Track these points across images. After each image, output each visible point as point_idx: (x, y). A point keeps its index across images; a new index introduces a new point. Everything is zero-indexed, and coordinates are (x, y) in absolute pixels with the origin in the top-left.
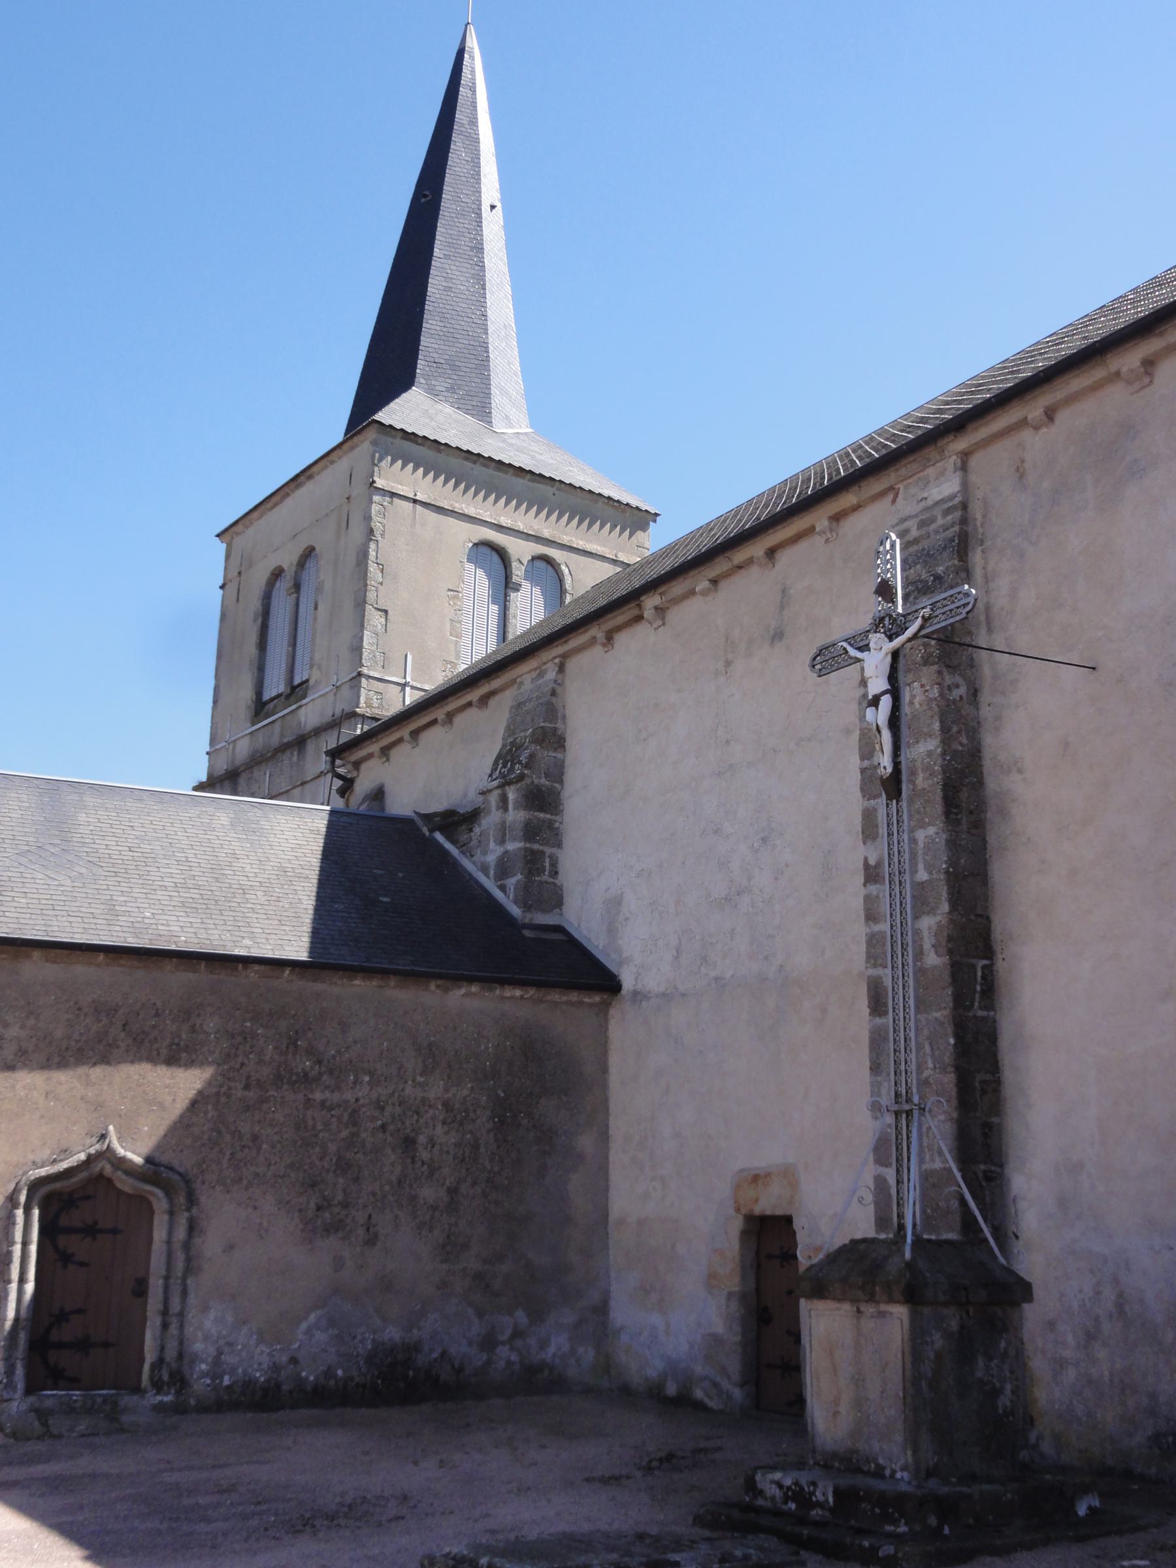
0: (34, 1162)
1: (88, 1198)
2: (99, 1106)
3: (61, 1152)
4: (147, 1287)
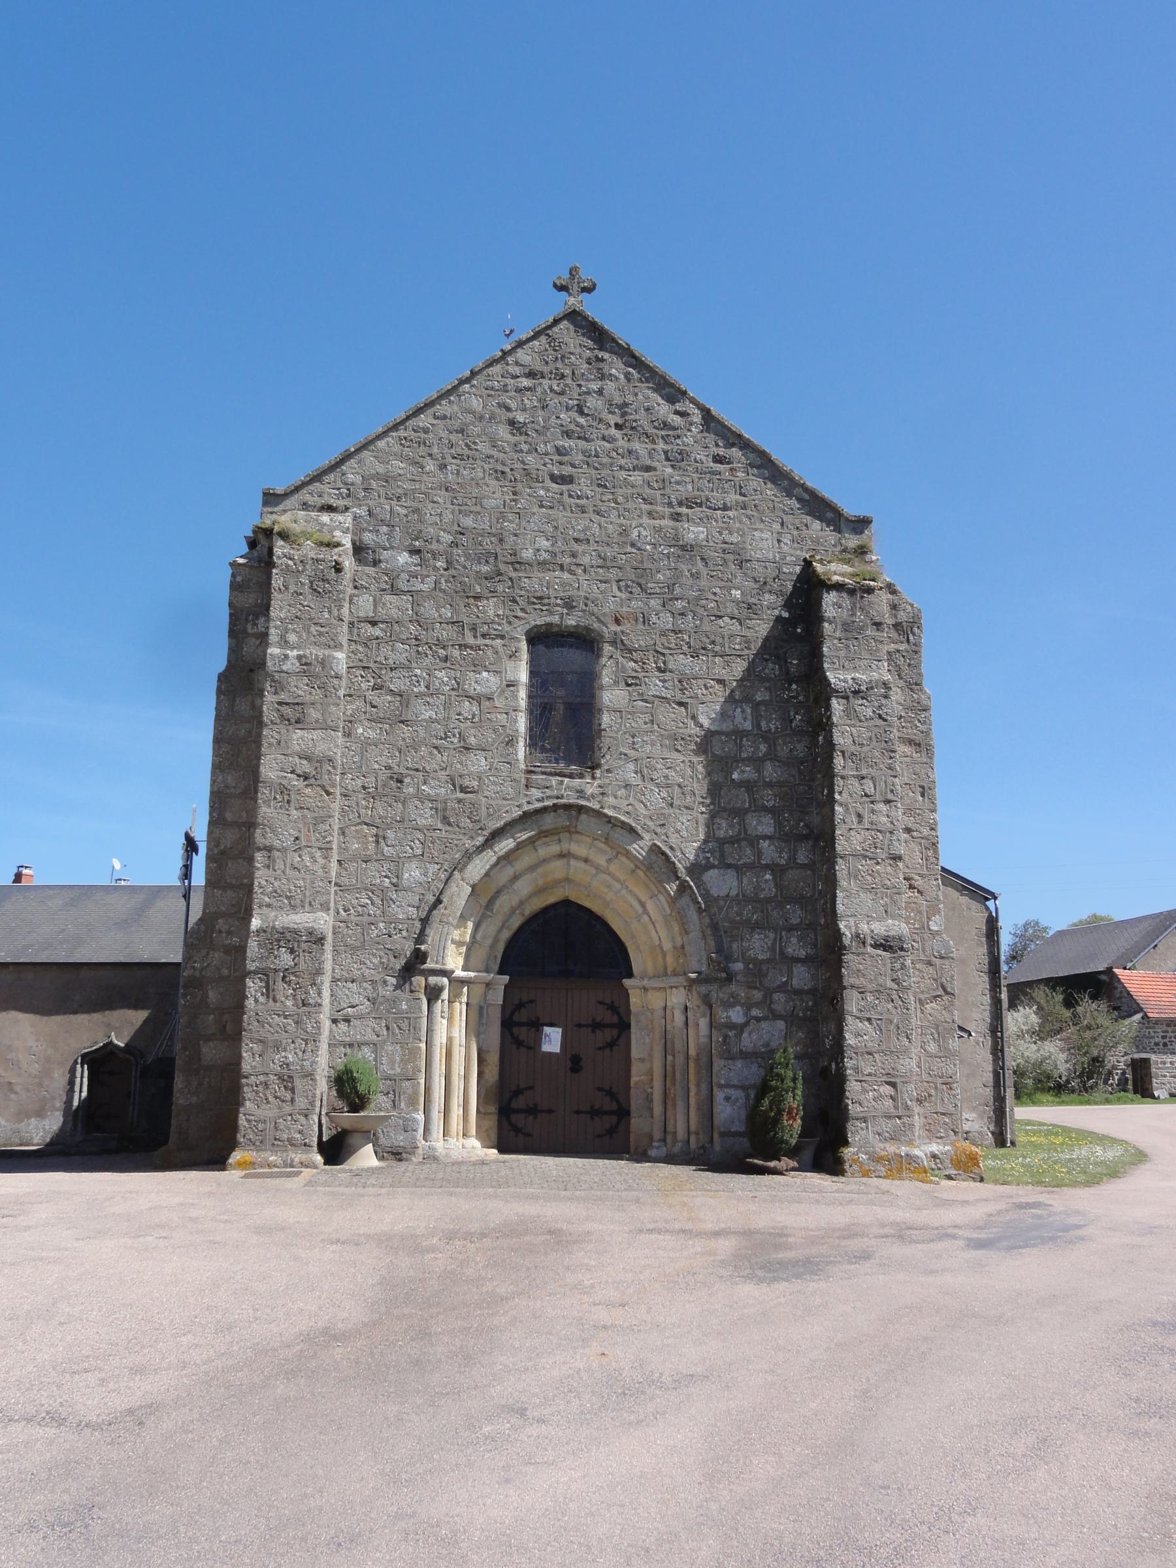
2: (108, 1025)
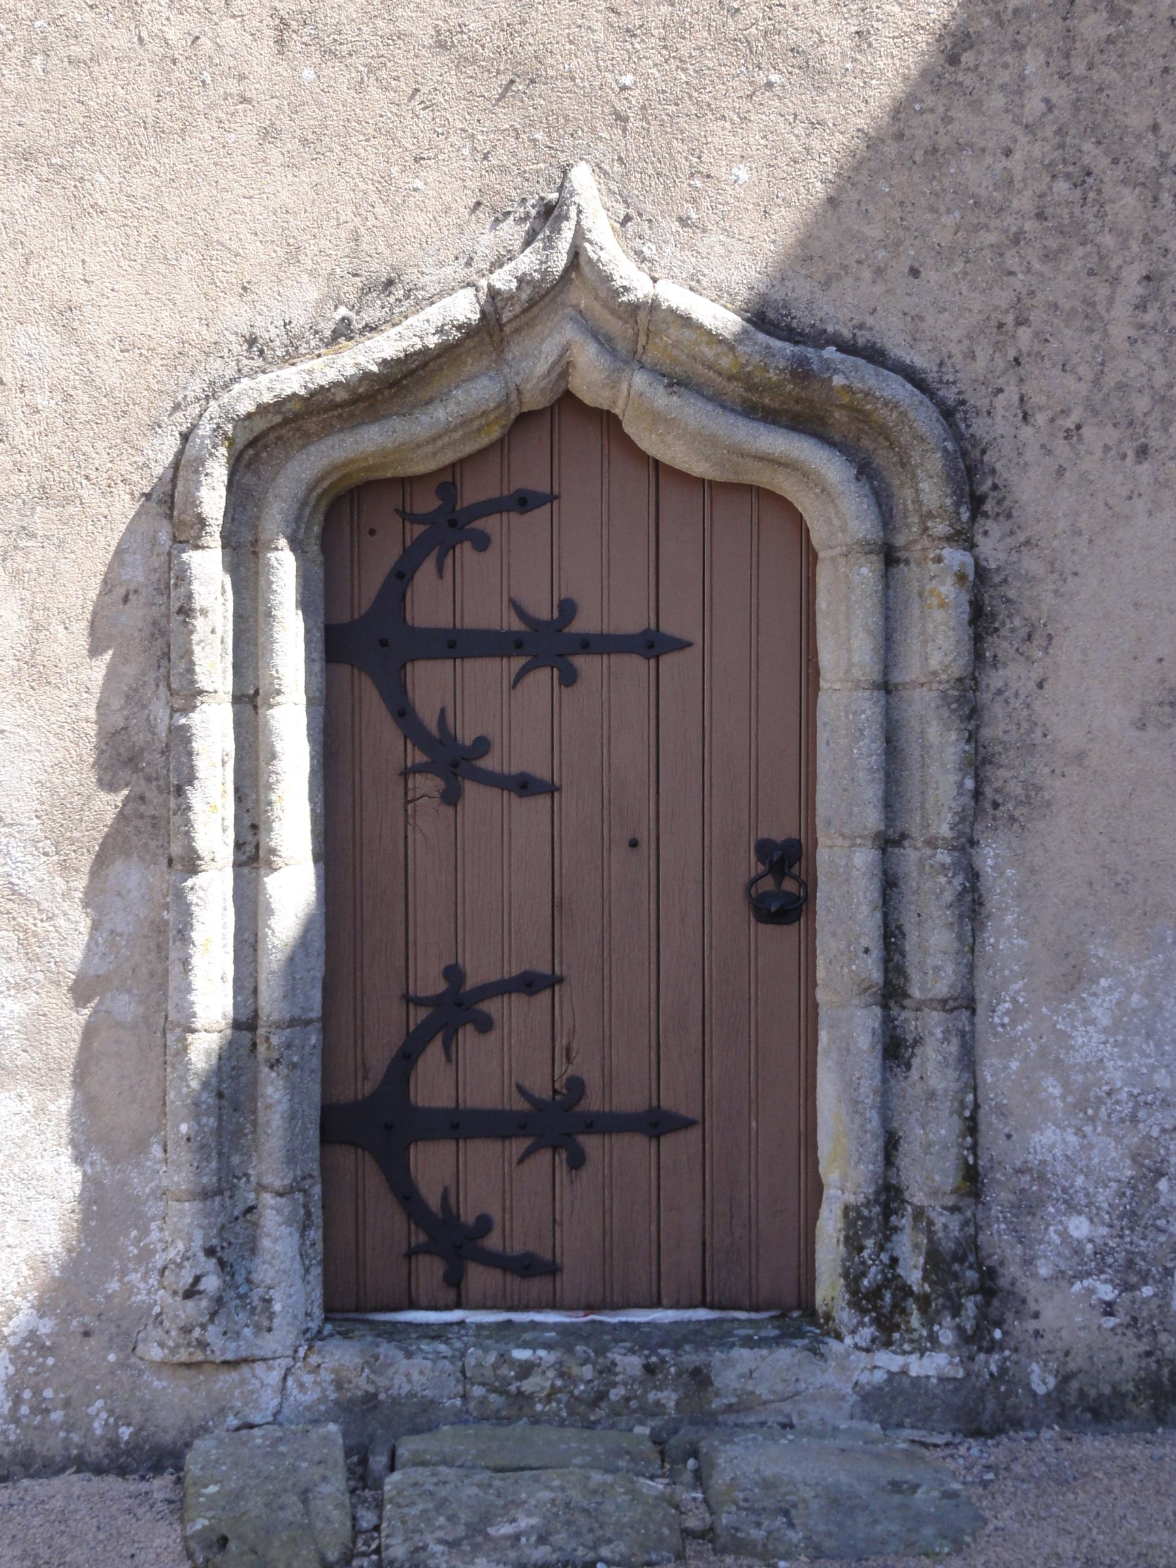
0: (252, 341)
1: (524, 502)
3: (366, 291)
4: (809, 887)
